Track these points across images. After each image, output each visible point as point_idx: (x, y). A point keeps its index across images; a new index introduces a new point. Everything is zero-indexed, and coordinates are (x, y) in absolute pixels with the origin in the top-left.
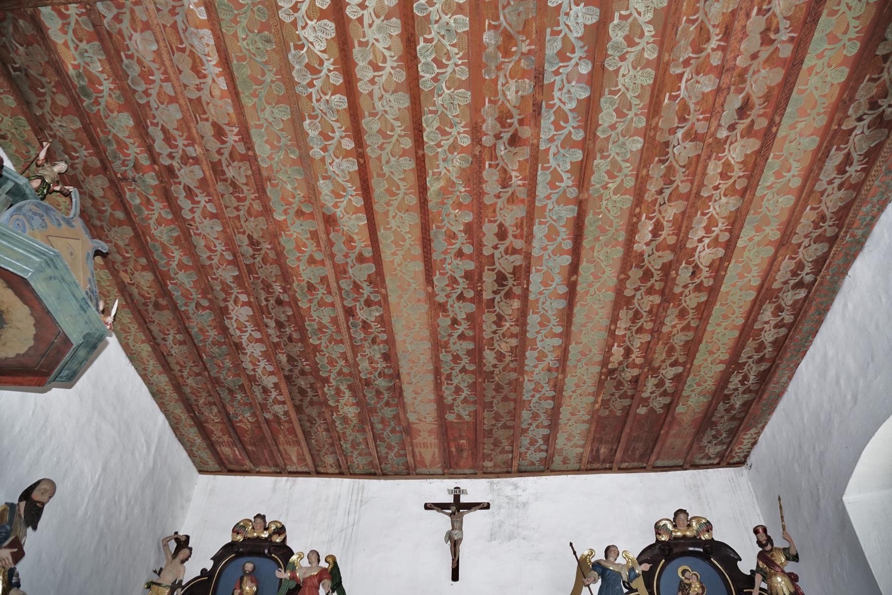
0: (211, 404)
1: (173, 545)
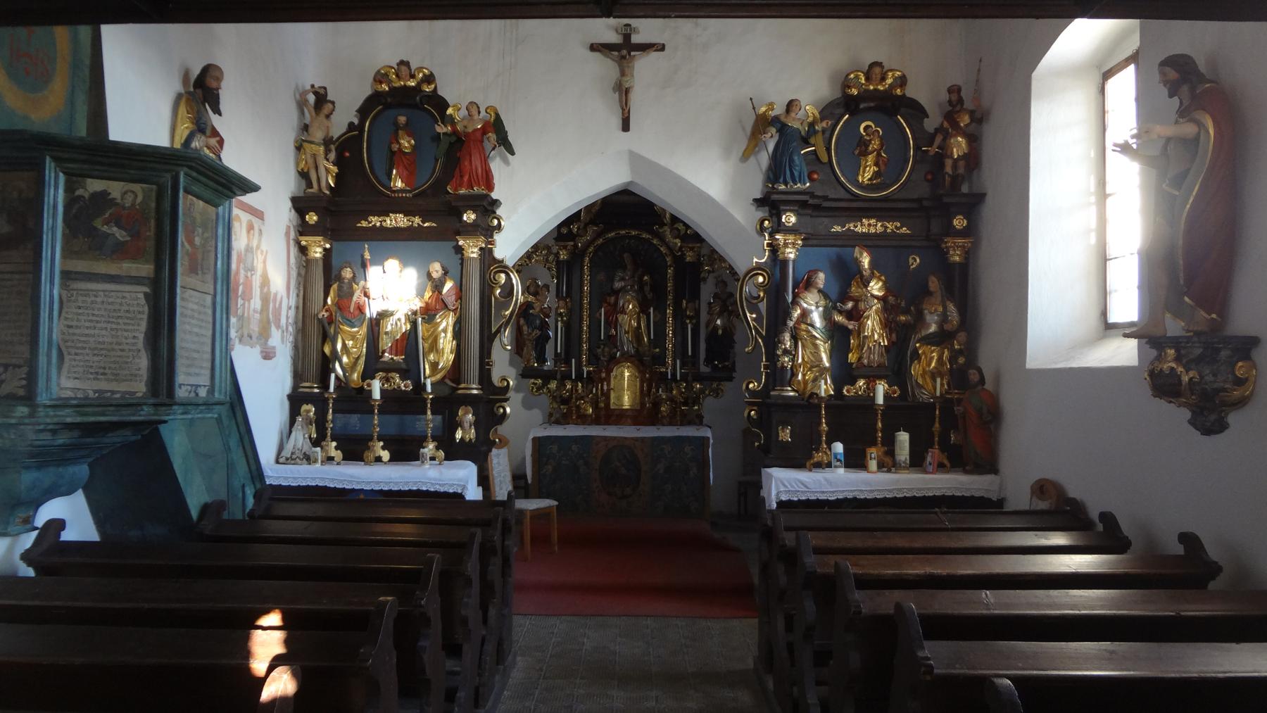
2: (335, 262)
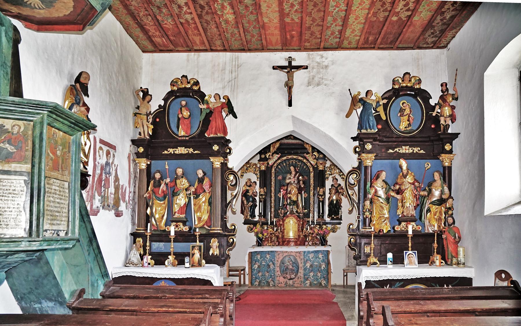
0: (147, 15)
1: (141, 94)
2: (153, 170)
